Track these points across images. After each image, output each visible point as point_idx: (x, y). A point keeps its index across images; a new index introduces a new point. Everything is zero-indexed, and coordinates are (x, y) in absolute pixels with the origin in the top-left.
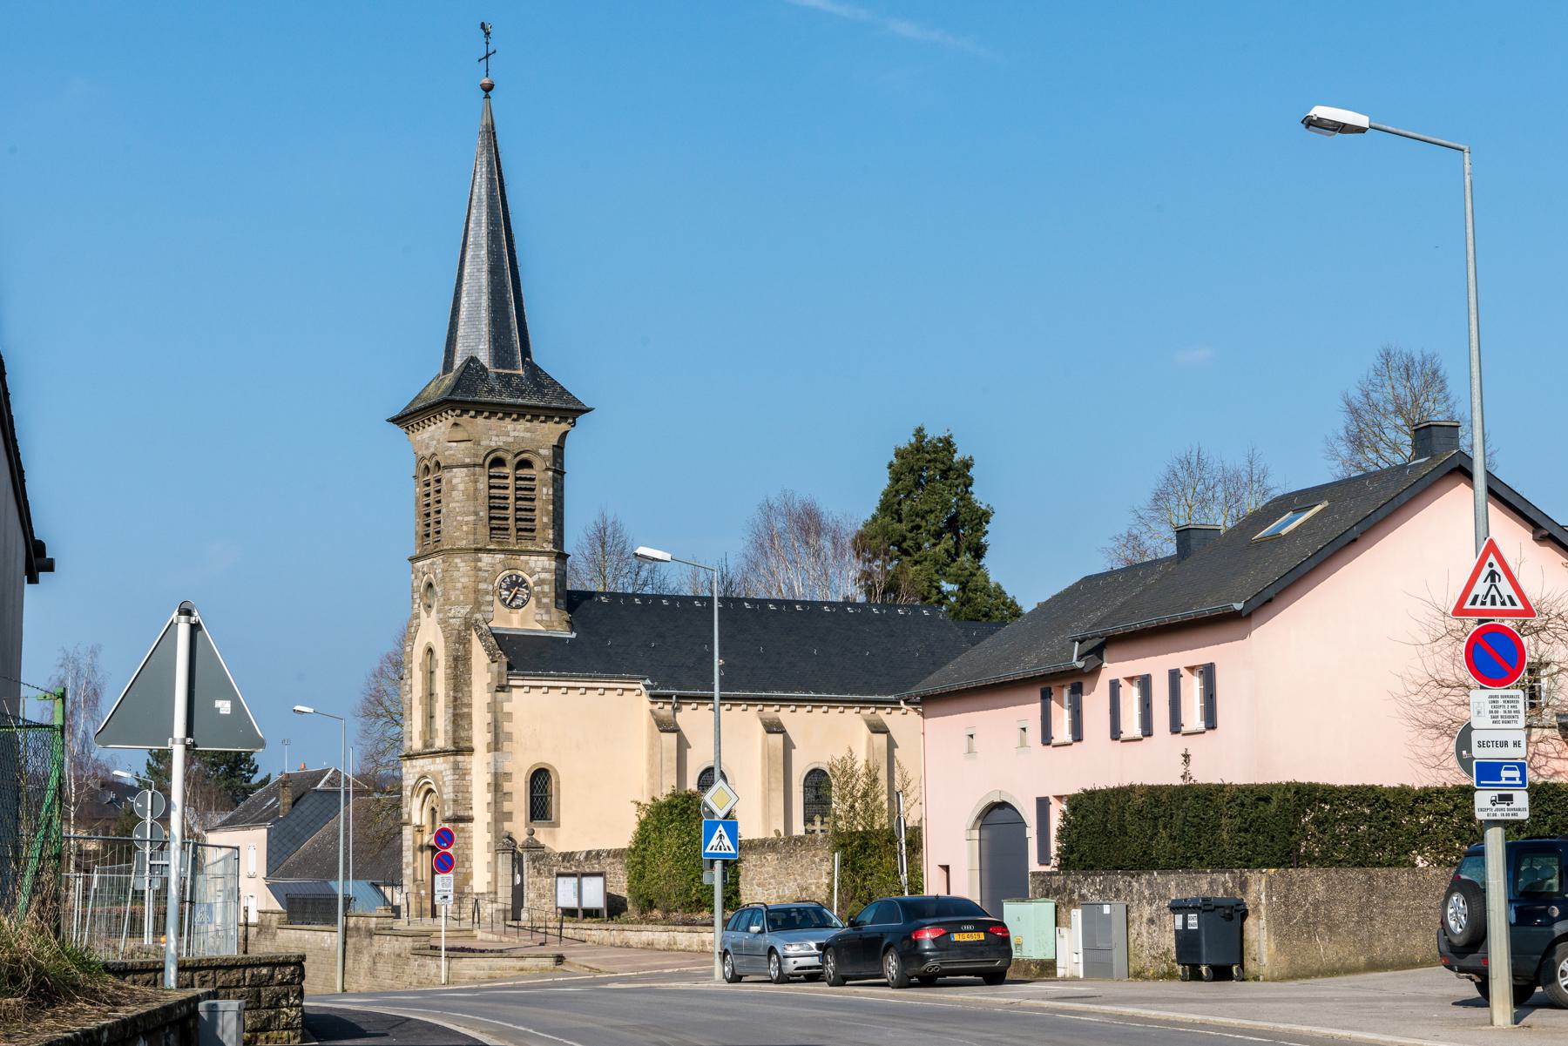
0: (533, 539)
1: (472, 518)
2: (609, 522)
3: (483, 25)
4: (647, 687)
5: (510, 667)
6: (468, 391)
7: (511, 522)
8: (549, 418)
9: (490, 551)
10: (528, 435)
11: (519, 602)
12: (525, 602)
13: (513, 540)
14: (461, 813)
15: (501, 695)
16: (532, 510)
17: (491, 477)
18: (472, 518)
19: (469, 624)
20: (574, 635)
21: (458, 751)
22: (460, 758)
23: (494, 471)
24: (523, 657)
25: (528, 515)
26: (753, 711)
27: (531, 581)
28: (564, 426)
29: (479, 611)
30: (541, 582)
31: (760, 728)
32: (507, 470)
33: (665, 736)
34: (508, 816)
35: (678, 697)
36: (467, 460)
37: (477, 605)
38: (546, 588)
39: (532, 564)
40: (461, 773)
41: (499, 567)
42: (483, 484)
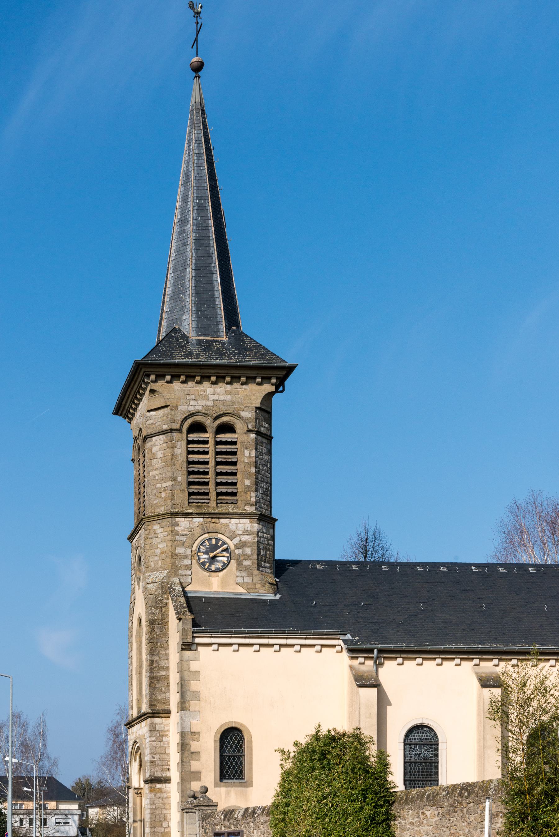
0: (235, 503)
1: (169, 484)
2: (370, 534)
3: (191, 5)
4: (345, 642)
5: (195, 624)
6: (164, 355)
7: (212, 486)
8: (250, 379)
9: (186, 515)
10: (229, 398)
11: (219, 565)
12: (225, 566)
13: (213, 504)
14: (158, 774)
15: (187, 653)
16: (235, 474)
17: (189, 442)
18: (169, 484)
19: (166, 589)
20: (278, 597)
21: (154, 714)
22: (157, 720)
23: (193, 436)
24: (211, 618)
25: (230, 479)
26: (468, 666)
27: (231, 544)
28: (268, 388)
29: (176, 575)
30: (242, 545)
31: (476, 684)
32: (208, 435)
33: (363, 690)
34: (196, 776)
35: (380, 651)
36: (165, 427)
37: (175, 569)
38: (248, 551)
40: (158, 735)
41: (198, 531)
42: (181, 449)
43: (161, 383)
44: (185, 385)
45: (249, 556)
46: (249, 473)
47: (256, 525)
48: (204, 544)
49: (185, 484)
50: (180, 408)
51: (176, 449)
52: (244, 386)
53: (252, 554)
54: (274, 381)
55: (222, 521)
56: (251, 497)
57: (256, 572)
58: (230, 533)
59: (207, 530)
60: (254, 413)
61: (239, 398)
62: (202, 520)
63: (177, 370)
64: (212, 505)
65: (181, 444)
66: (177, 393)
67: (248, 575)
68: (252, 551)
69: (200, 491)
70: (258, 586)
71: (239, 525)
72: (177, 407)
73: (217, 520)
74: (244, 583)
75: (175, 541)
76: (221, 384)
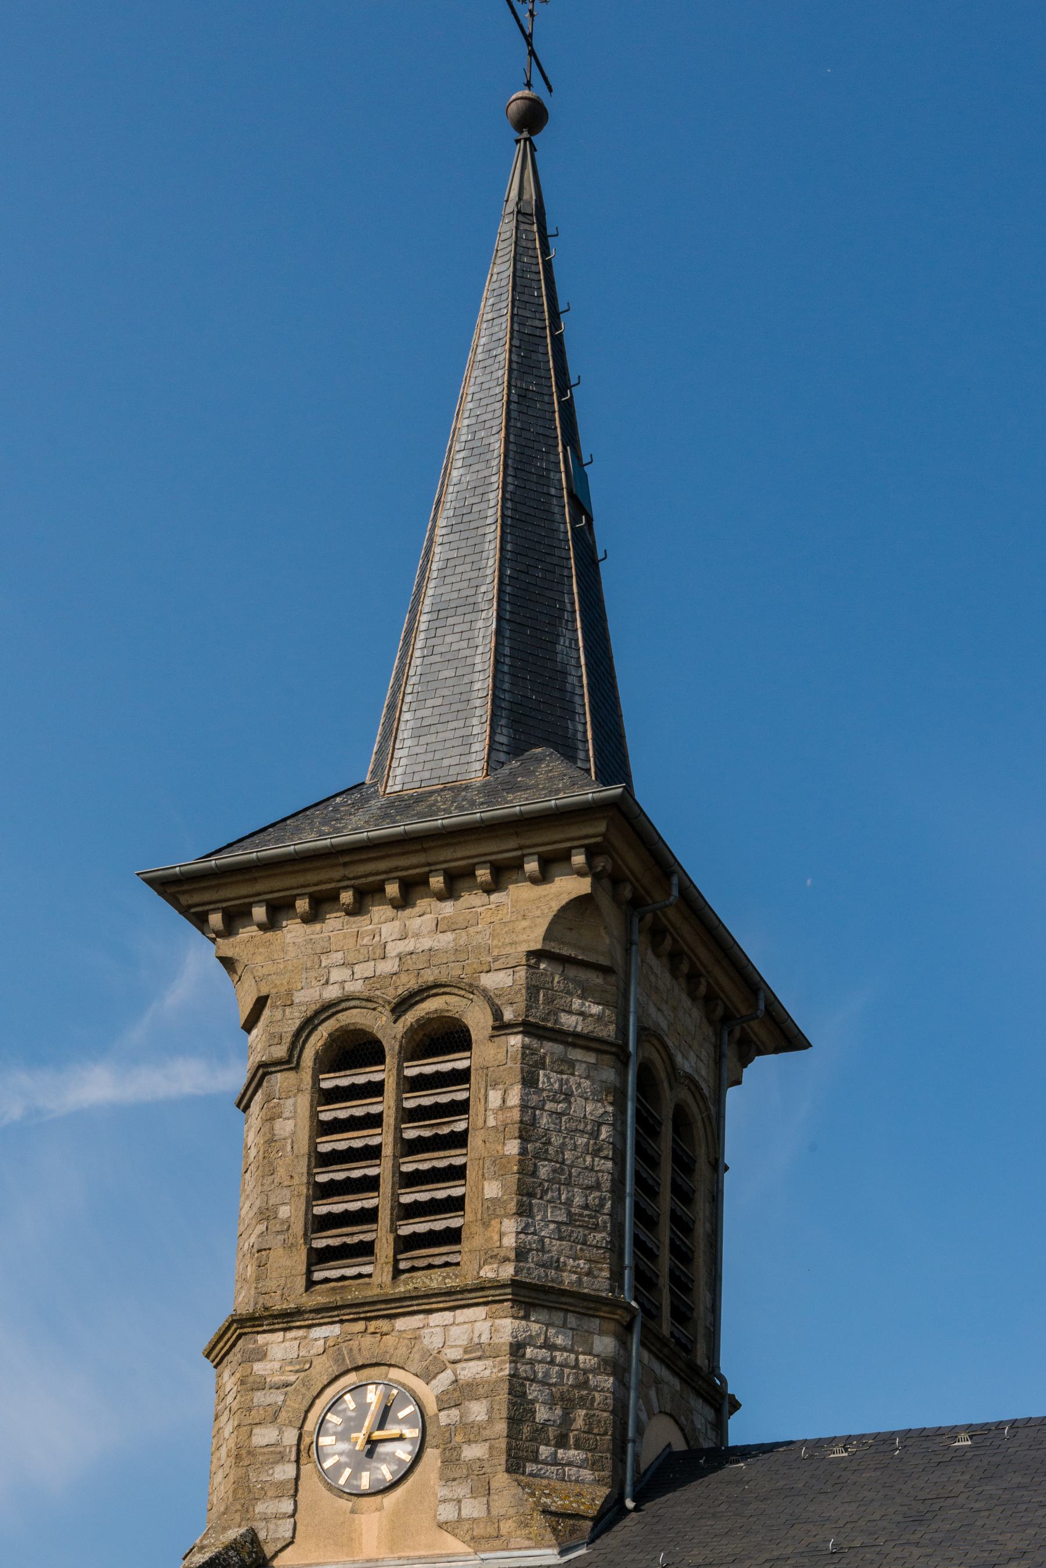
8: (503, 874)
39: (432, 1339)
43: (247, 933)
44: (317, 927)
45: (481, 1427)
46: (500, 1160)
47: (508, 1321)
48: (340, 1407)
49: (298, 1228)
50: (298, 997)
51: (278, 1124)
52: (494, 897)
53: (490, 1420)
54: (579, 859)
55: (401, 1324)
56: (501, 1235)
57: (501, 1479)
58: (423, 1358)
59: (352, 1359)
60: (522, 973)
61: (480, 935)
62: (336, 1329)
63: (276, 883)
64: (377, 1274)
65: (295, 1105)
66: (292, 952)
67: (474, 1493)
68: (490, 1411)
69: (349, 1240)
70: (506, 1527)
71: (453, 1329)
72: (289, 993)
73: (384, 1325)
74: (460, 1520)
75: (250, 1410)
76: (422, 904)
